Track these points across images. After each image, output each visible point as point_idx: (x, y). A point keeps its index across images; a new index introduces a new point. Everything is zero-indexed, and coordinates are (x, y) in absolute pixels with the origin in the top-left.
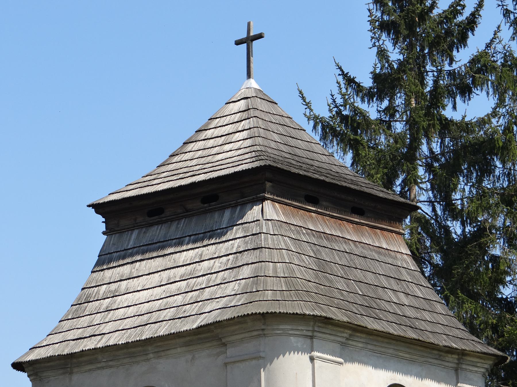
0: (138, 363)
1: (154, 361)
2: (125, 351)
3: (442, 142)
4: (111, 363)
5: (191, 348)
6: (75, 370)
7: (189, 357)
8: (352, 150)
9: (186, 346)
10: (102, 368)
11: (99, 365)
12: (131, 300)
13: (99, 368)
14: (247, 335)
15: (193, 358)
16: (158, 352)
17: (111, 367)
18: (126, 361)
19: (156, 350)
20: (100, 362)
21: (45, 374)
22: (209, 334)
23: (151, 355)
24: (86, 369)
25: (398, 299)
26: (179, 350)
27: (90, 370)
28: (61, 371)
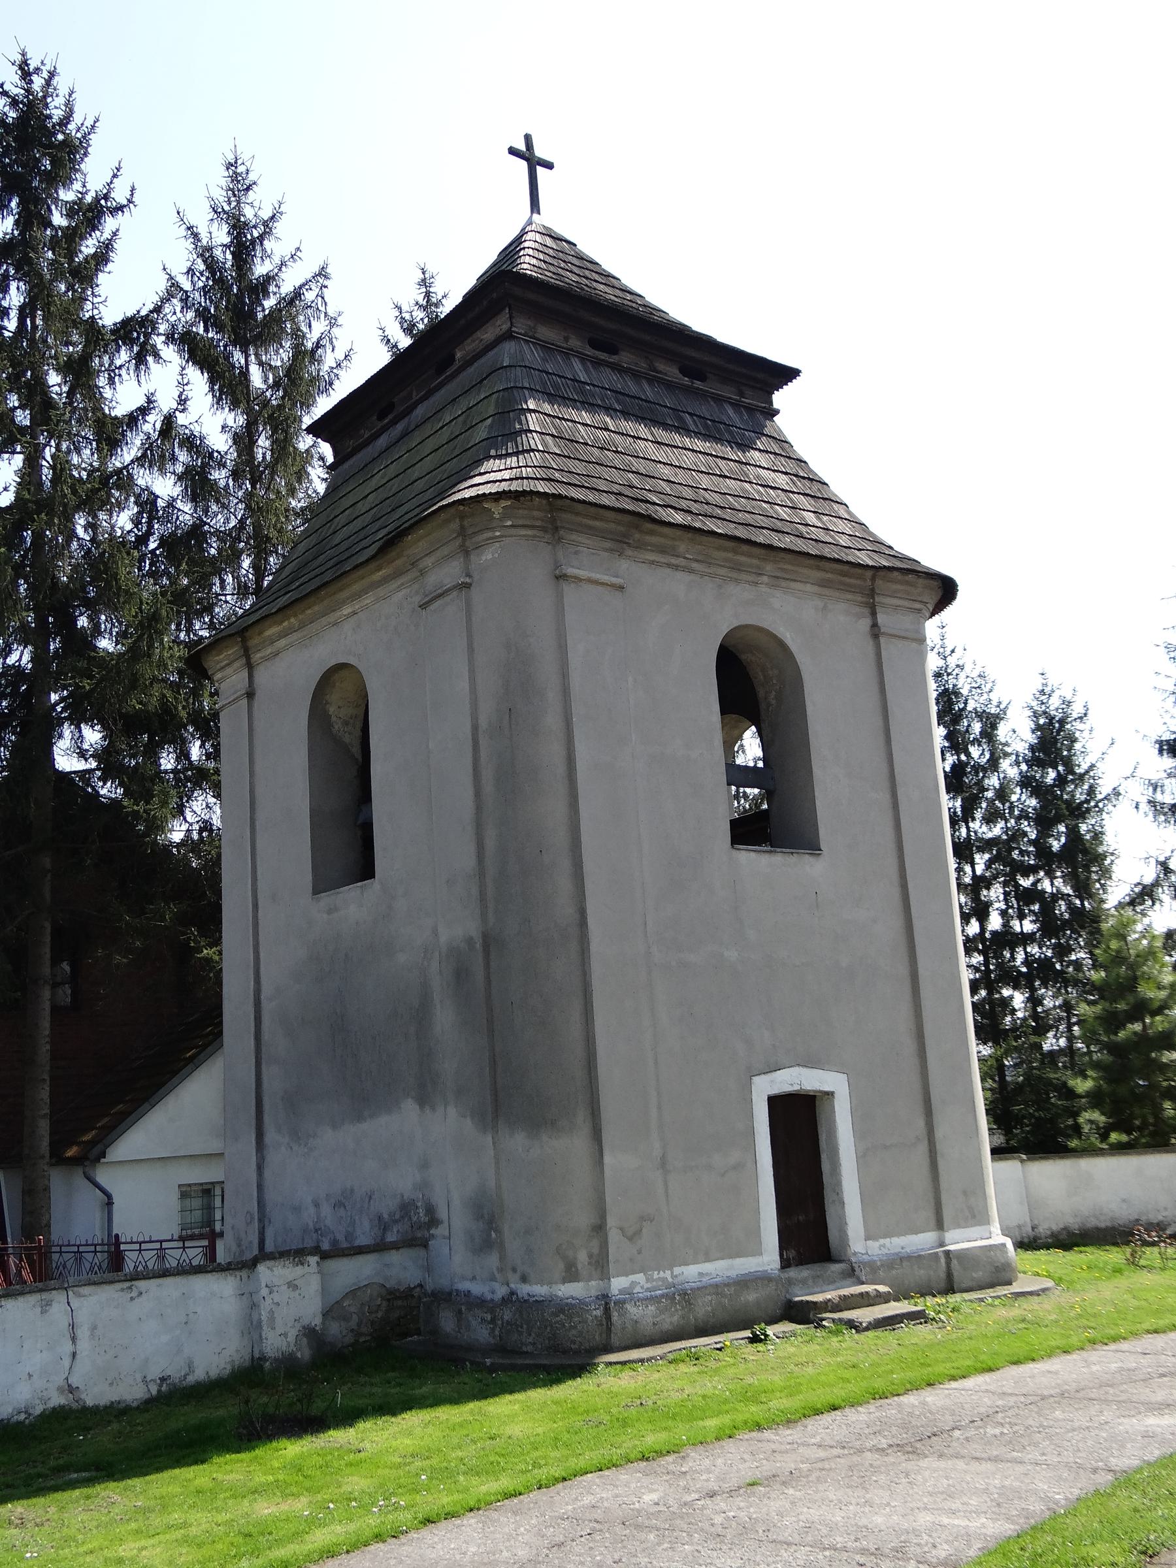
0: (737, 581)
1: (764, 590)
2: (730, 555)
3: (156, 549)
4: (695, 565)
5: (826, 591)
6: (629, 552)
7: (819, 603)
8: (128, 651)
9: (819, 586)
10: (676, 567)
11: (674, 561)
12: (959, 1418)
13: (669, 565)
14: (906, 603)
15: (825, 608)
16: (777, 577)
17: (691, 571)
18: (723, 571)
19: (779, 575)
20: (677, 556)
21: (574, 537)
22: (858, 582)
23: (765, 579)
24: (647, 557)
25: (823, 523)
26: (809, 587)
27: (652, 562)
28: (608, 544)
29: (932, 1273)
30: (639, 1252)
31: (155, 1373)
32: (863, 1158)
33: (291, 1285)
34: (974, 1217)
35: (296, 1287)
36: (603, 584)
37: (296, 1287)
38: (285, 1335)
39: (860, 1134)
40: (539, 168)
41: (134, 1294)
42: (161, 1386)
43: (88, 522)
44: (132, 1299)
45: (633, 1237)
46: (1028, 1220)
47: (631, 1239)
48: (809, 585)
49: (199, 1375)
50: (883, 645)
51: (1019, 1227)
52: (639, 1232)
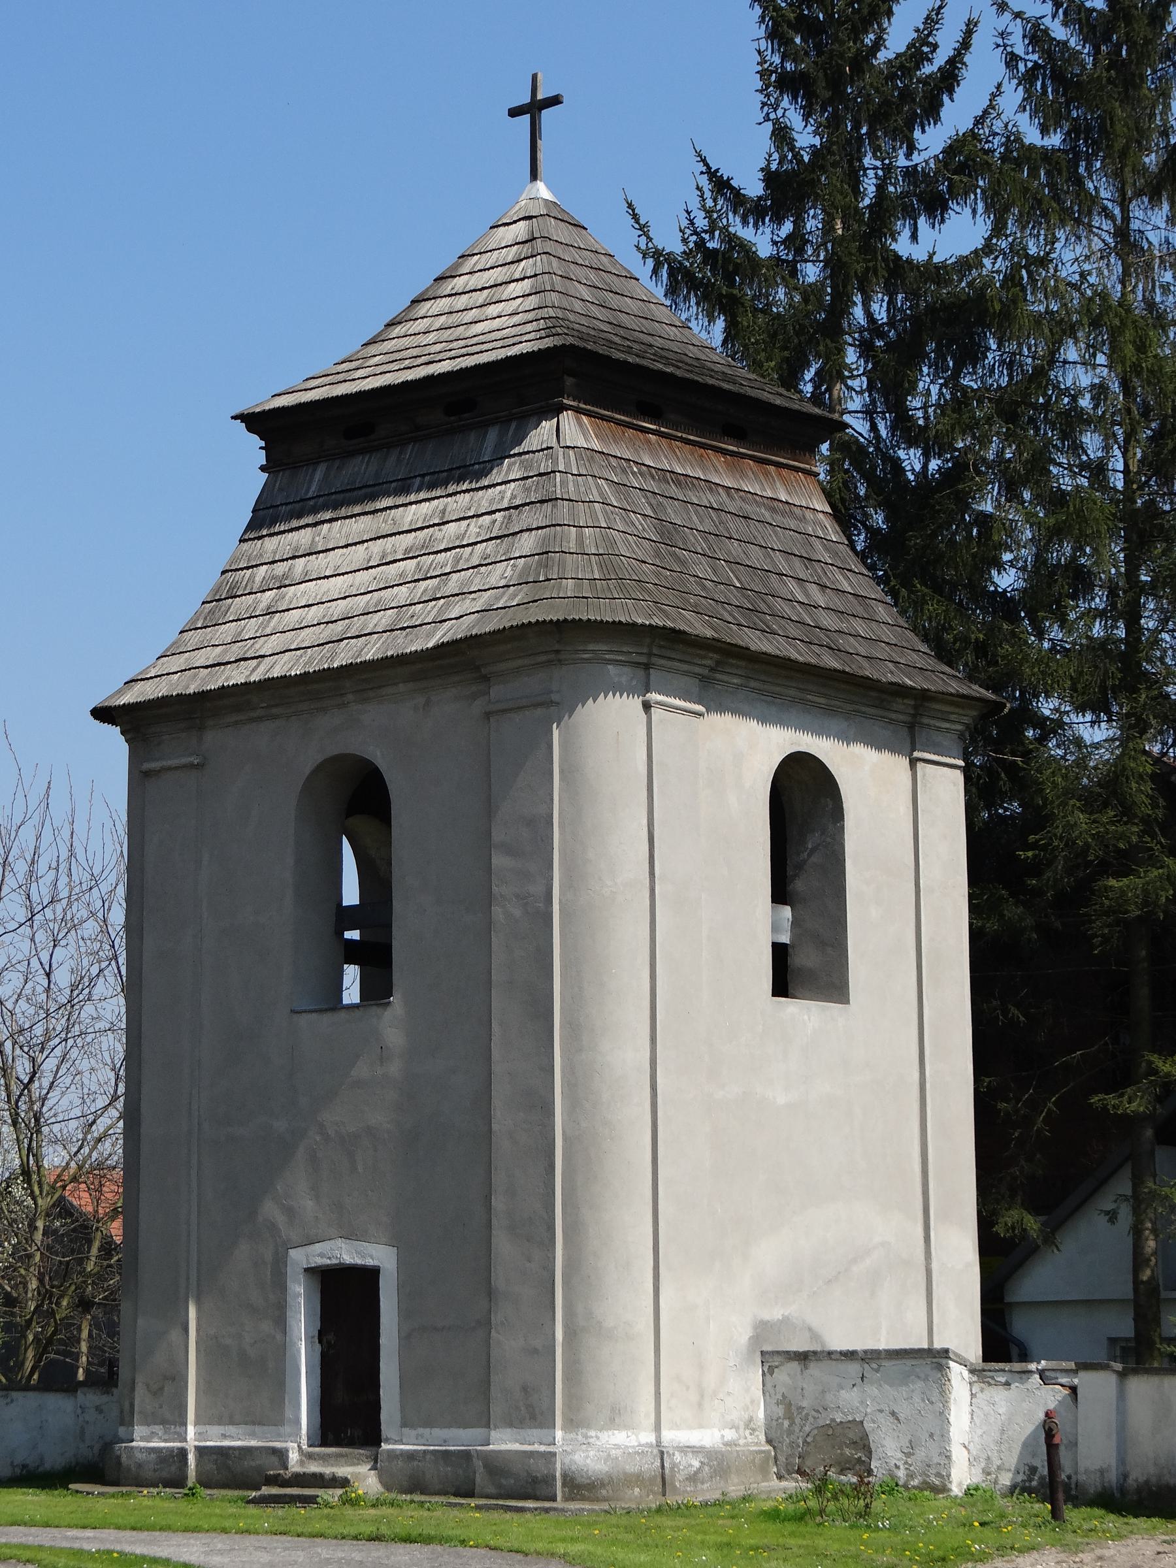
4: (274, 711)
10: (259, 719)
14: (526, 661)
17: (275, 717)
23: (350, 697)
26: (402, 687)
27: (236, 723)
29: (460, 1472)
30: (161, 1407)
31: (19, 1460)
32: (406, 1339)
33: (99, 1409)
34: (533, 1417)
35: (101, 1412)
36: (176, 768)
37: (101, 1412)
38: (91, 1447)
39: (405, 1314)
40: (540, 97)
41: (9, 1400)
42: (22, 1470)
43: (979, 421)
44: (7, 1404)
45: (157, 1393)
46: (1114, 1463)
47: (155, 1394)
48: (401, 685)
49: (47, 1466)
50: (652, 678)
51: (1102, 1472)
52: (162, 1389)
